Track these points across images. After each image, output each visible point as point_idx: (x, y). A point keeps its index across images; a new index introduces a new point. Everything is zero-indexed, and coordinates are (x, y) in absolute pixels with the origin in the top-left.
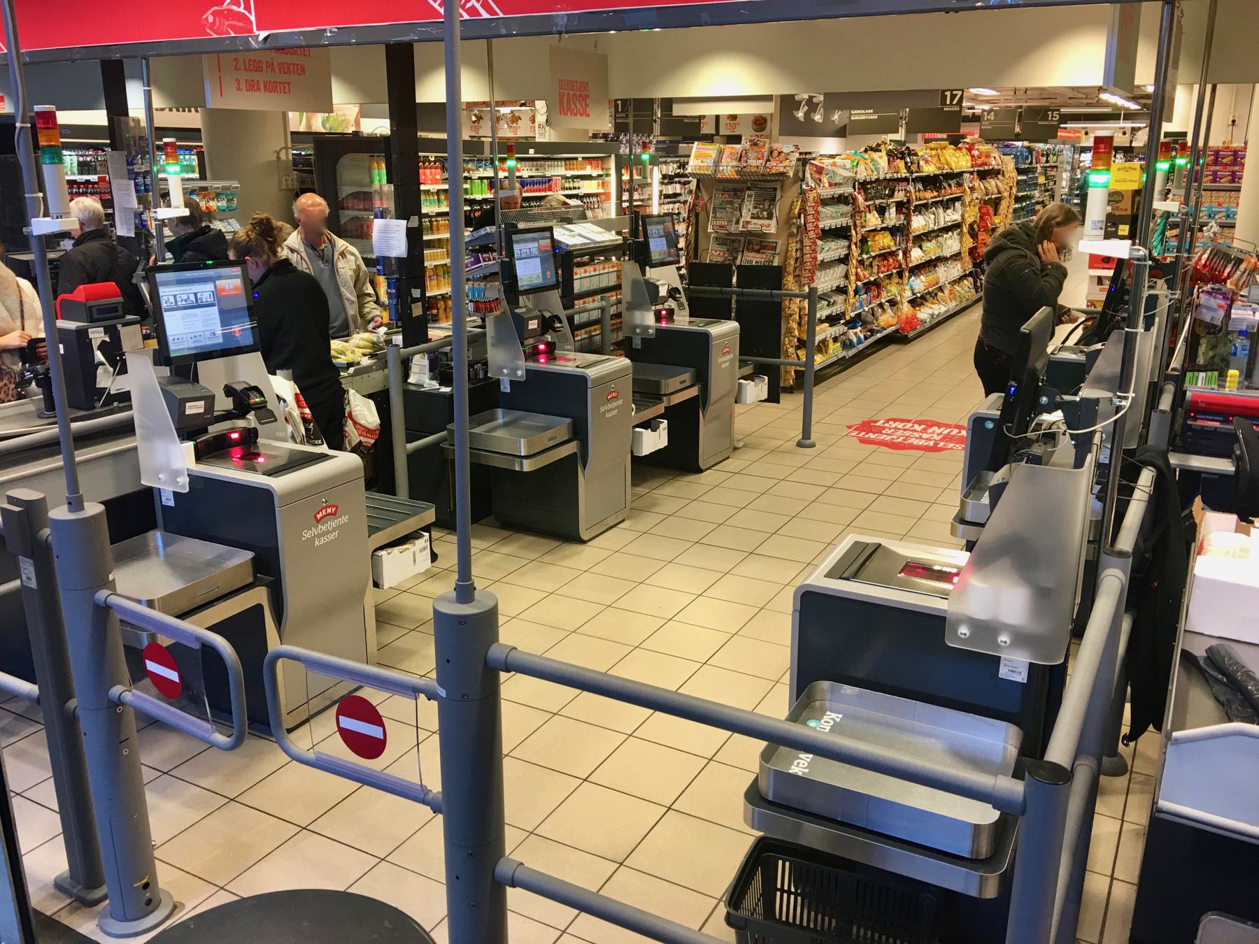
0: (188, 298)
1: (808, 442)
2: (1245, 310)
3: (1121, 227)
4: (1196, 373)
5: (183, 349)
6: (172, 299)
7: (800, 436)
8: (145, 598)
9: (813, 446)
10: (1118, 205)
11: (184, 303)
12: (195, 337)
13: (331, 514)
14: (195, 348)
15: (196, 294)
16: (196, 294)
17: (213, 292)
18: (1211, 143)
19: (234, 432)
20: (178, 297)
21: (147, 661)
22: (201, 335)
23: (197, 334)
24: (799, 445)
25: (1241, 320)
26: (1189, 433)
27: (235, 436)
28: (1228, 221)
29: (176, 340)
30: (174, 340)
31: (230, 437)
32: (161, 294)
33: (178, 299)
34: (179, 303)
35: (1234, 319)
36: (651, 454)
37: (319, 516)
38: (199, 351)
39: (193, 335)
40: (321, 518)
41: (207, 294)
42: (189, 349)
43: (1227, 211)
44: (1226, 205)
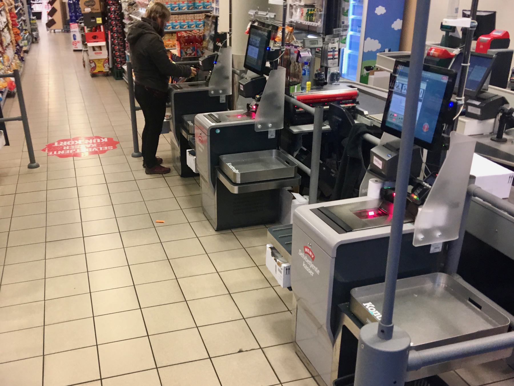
1: (34, 165)
2: (305, 52)
3: (98, 19)
4: (294, 86)
7: (29, 162)
8: (286, 271)
9: (38, 166)
10: (94, 7)
20: (404, 86)
24: (30, 167)
25: (305, 57)
26: (295, 116)
28: (179, 11)
29: (392, 116)
30: (391, 115)
34: (403, 91)
35: (303, 57)
36: (189, 167)
43: (179, 6)
44: (169, 3)
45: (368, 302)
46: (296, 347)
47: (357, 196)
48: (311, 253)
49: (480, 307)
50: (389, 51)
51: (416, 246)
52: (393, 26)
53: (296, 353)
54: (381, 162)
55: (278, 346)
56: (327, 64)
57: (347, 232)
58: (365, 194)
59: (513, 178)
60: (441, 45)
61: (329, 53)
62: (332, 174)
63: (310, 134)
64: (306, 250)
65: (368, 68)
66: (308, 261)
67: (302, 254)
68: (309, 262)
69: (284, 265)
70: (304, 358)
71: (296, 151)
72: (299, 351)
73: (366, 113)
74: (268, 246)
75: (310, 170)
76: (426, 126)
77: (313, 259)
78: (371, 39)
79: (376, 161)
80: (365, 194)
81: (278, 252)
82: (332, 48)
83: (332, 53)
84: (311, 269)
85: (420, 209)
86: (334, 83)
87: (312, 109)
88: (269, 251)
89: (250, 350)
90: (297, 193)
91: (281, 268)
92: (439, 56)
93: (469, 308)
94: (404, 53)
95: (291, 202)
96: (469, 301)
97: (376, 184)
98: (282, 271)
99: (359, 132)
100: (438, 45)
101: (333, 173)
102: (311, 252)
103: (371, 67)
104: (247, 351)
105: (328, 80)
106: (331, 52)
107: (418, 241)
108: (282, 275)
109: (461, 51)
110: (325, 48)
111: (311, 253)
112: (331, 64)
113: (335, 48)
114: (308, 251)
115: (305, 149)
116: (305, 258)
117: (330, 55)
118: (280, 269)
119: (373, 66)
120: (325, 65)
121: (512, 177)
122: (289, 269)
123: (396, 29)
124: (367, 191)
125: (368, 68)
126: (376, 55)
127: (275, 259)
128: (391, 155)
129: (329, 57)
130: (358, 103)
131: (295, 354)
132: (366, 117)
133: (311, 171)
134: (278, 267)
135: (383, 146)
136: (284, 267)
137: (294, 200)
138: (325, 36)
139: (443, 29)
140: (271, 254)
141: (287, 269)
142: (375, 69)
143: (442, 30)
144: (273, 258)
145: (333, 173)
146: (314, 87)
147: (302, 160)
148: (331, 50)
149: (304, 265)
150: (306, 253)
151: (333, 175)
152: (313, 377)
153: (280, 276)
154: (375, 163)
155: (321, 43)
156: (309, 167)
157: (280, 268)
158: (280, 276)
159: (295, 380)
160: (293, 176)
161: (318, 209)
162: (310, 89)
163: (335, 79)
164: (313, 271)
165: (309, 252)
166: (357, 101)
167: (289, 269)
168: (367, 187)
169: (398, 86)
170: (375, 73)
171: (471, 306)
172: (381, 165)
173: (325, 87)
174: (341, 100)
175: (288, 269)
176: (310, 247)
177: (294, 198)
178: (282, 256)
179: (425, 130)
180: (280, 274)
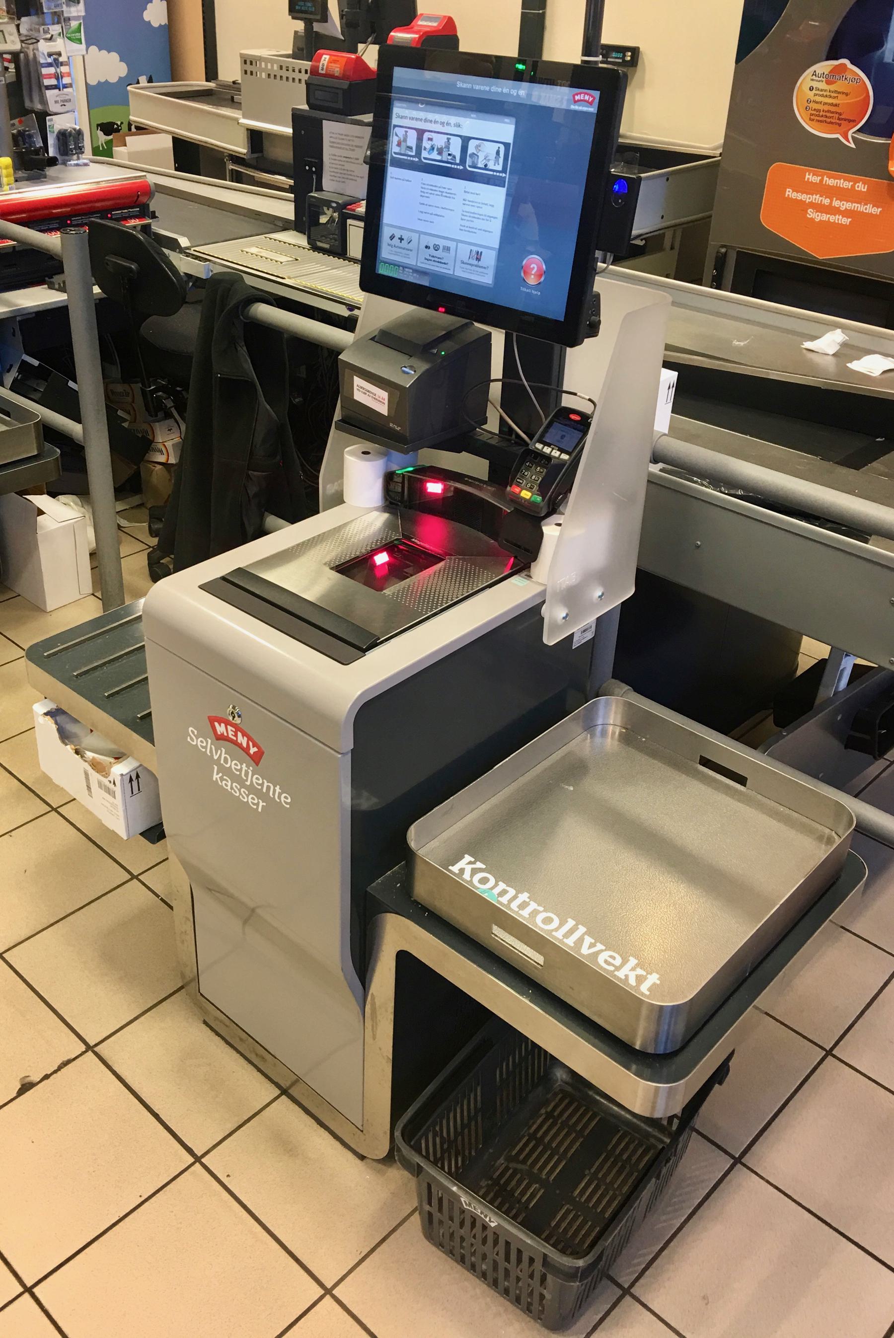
0: (448, 146)
5: (404, 267)
6: (412, 141)
11: (435, 155)
12: (436, 248)
13: (587, 102)
14: (423, 273)
15: (466, 140)
16: (466, 140)
17: (507, 145)
18: (542, 964)
19: (436, 479)
20: (426, 135)
21: (355, 377)
22: (447, 249)
23: (442, 243)
27: (435, 488)
29: (396, 241)
30: (392, 237)
31: (426, 489)
32: (395, 121)
33: (426, 144)
34: (424, 154)
37: (577, 98)
38: (425, 282)
39: (432, 241)
40: (579, 101)
41: (491, 149)
42: (416, 271)
45: (458, 858)
46: (201, 1008)
47: (314, 510)
48: (243, 741)
49: (742, 780)
50: (150, 80)
51: (551, 644)
52: (147, 16)
53: (205, 1023)
54: (384, 395)
55: (143, 1018)
56: (44, 101)
57: (364, 651)
58: (338, 499)
59: (674, 389)
60: (294, 56)
61: (44, 71)
62: (123, 422)
63: (59, 314)
64: (221, 729)
65: (108, 128)
66: (233, 764)
67: (205, 744)
68: (242, 767)
69: (121, 769)
70: (241, 1040)
71: (8, 371)
72: (216, 1019)
73: (184, 242)
74: (40, 708)
75: (80, 426)
76: (535, 263)
77: (256, 759)
78: (100, 50)
79: (367, 392)
80: (338, 499)
81: (75, 721)
82: (50, 55)
83: (52, 70)
84: (252, 789)
85: (549, 530)
86: (72, 162)
87: (52, 241)
88: (47, 728)
89: (55, 1072)
90: (41, 493)
91: (111, 778)
92: (344, 77)
93: (716, 789)
94: (191, 85)
95: (34, 527)
96: (700, 764)
97: (368, 463)
98: (118, 789)
99: (232, 303)
100: (288, 56)
101: (125, 420)
102: (244, 734)
103: (115, 124)
104: (47, 1077)
105: (52, 152)
106: (50, 65)
107: (555, 627)
108: (119, 800)
109: (100, 130)
110: (26, 56)
111: (243, 741)
112: (56, 102)
113: (59, 54)
114: (230, 733)
115: (36, 363)
116: (222, 754)
117: (49, 76)
118: (107, 783)
119: (119, 123)
120: (38, 107)
121: (673, 386)
122: (138, 776)
123: (155, 24)
124: (342, 485)
125: (108, 128)
126: (127, 92)
127: (77, 752)
128: (411, 367)
129: (47, 82)
130: (153, 216)
131: (204, 1026)
132: (188, 255)
133: (84, 428)
134: (94, 776)
135: (373, 339)
136: (122, 775)
137: (40, 519)
138: (19, 19)
139: (296, 15)
140: (56, 735)
141: (131, 780)
142: (125, 128)
143: (293, 18)
144: (69, 748)
145: (125, 420)
146: (20, 174)
147: (37, 396)
148: (50, 60)
149: (216, 777)
150: (220, 738)
151: (126, 425)
152: (284, 1092)
153: (112, 804)
154: (358, 396)
155: (12, 38)
156: (78, 420)
157: (105, 781)
158: (112, 804)
159: (236, 1125)
160: (36, 453)
161: (223, 578)
162: (13, 178)
163: (71, 150)
164: (259, 794)
165: (236, 736)
166: (151, 209)
167: (138, 776)
168: (339, 474)
169: (405, 140)
170: (128, 139)
171: (715, 780)
172: (386, 402)
173: (51, 171)
174: (69, 216)
175: (134, 778)
176: (238, 721)
177: (41, 512)
178: (92, 731)
179: (532, 280)
180: (109, 798)
